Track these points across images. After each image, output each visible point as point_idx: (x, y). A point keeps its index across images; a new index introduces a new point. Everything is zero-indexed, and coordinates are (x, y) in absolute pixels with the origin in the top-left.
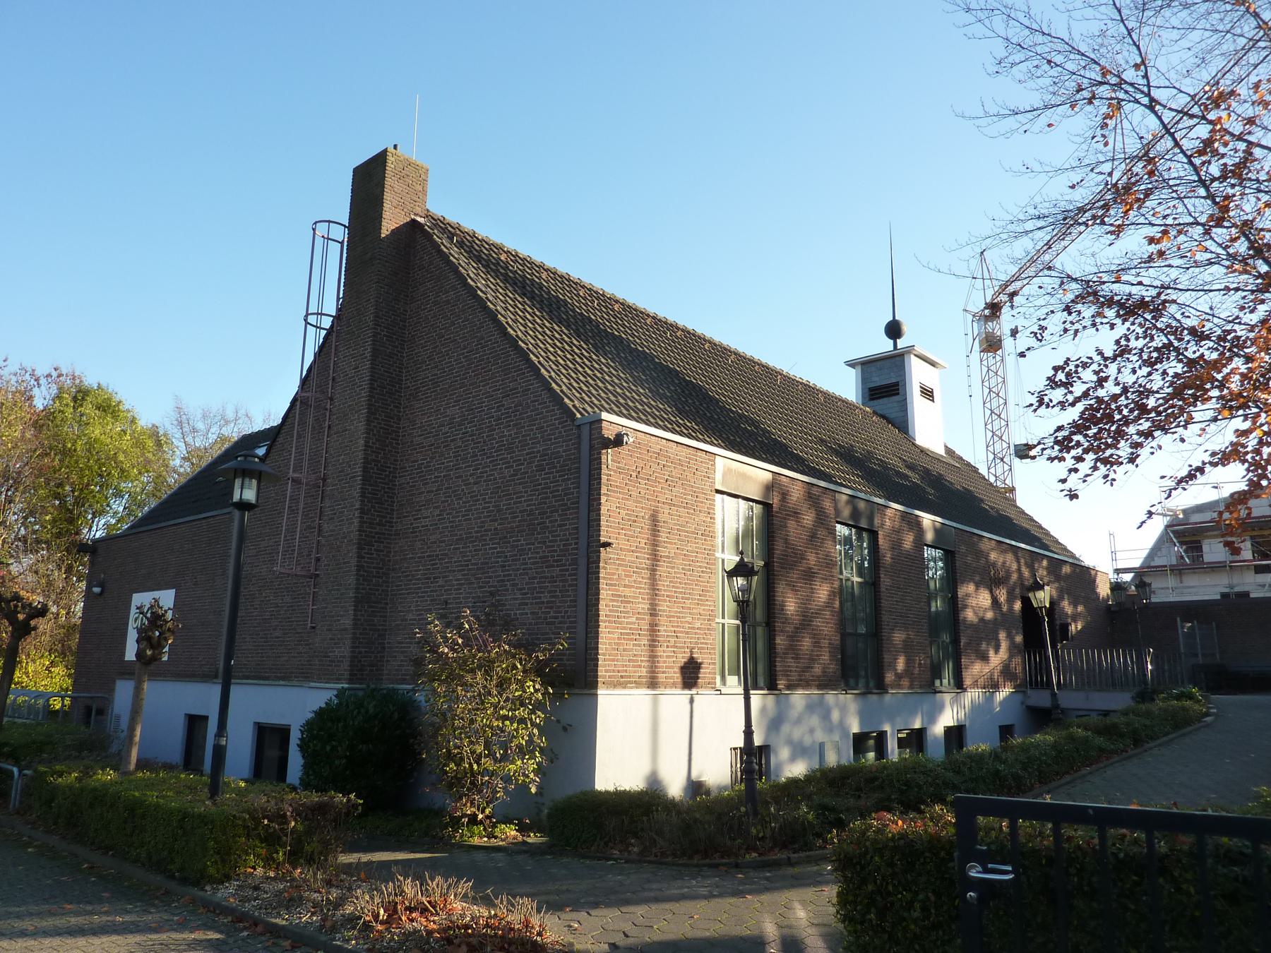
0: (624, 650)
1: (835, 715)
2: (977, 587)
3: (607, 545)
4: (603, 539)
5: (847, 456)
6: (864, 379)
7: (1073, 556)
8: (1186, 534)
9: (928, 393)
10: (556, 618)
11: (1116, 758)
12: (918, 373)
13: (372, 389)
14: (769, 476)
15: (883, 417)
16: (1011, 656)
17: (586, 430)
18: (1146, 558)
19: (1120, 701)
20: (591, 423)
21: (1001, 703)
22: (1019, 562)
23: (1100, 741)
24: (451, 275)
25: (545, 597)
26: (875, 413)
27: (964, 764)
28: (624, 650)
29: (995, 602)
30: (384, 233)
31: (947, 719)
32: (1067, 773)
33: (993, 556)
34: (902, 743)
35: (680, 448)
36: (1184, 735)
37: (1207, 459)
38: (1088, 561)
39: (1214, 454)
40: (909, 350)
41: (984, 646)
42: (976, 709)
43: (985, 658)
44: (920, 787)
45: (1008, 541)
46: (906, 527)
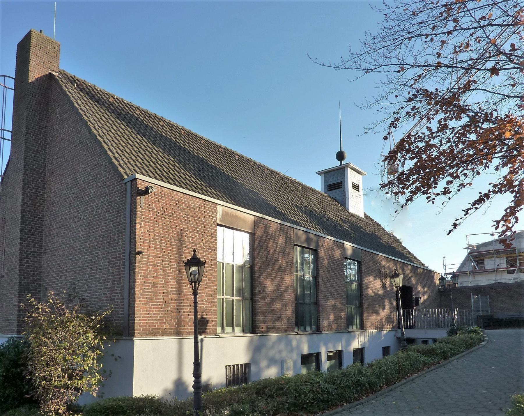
0: (154, 314)
1: (294, 343)
2: (375, 278)
3: (140, 253)
4: (137, 250)
5: (311, 215)
6: (325, 181)
7: (424, 265)
8: (477, 256)
9: (356, 187)
10: (115, 296)
11: (433, 367)
12: (352, 177)
13: (25, 169)
14: (253, 218)
15: (334, 199)
16: (391, 312)
17: (129, 184)
18: (459, 268)
19: (441, 334)
20: (132, 181)
21: (384, 335)
22: (396, 267)
23: (424, 358)
24: (67, 103)
25: (110, 285)
26: (329, 197)
27: (338, 377)
28: (154, 314)
29: (384, 286)
30: (31, 80)
31: (356, 344)
32: (404, 378)
33: (383, 263)
34: (329, 358)
35: (193, 199)
36: (470, 352)
37: (491, 189)
38: (431, 268)
39: (495, 186)
40: (347, 165)
41: (377, 307)
42: (372, 337)
43: (378, 313)
44: (306, 394)
45: (391, 257)
46: (335, 248)
